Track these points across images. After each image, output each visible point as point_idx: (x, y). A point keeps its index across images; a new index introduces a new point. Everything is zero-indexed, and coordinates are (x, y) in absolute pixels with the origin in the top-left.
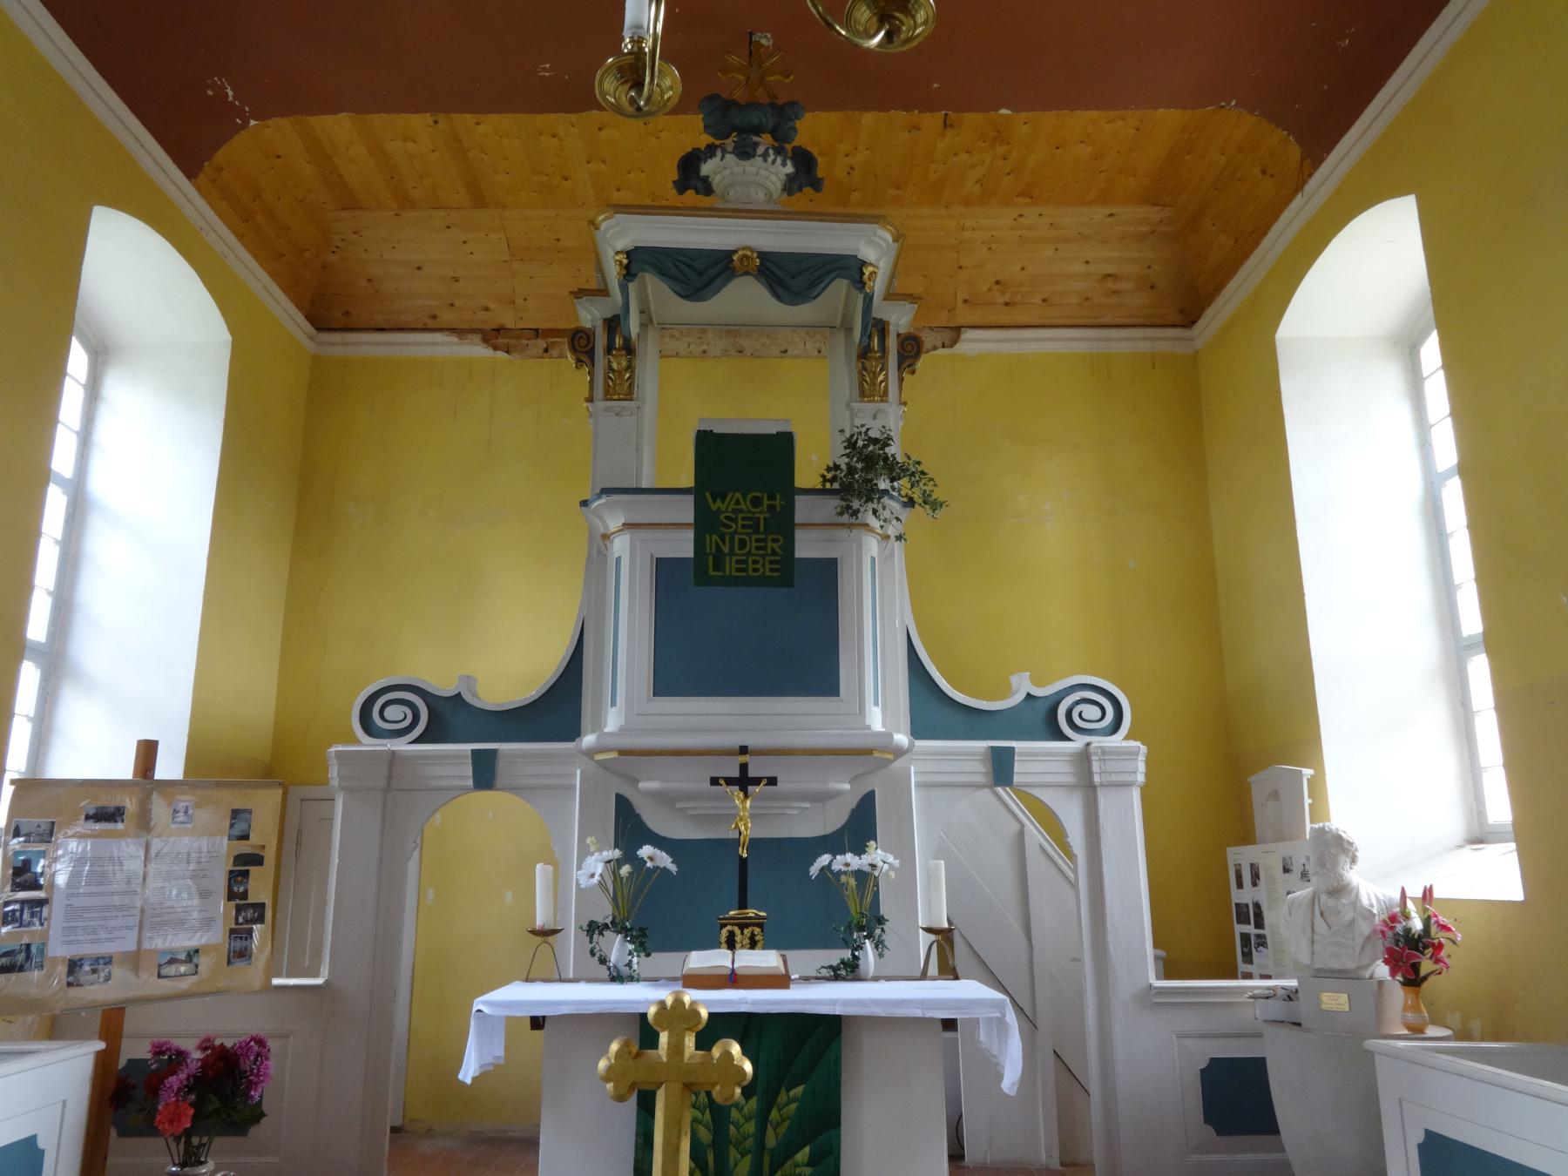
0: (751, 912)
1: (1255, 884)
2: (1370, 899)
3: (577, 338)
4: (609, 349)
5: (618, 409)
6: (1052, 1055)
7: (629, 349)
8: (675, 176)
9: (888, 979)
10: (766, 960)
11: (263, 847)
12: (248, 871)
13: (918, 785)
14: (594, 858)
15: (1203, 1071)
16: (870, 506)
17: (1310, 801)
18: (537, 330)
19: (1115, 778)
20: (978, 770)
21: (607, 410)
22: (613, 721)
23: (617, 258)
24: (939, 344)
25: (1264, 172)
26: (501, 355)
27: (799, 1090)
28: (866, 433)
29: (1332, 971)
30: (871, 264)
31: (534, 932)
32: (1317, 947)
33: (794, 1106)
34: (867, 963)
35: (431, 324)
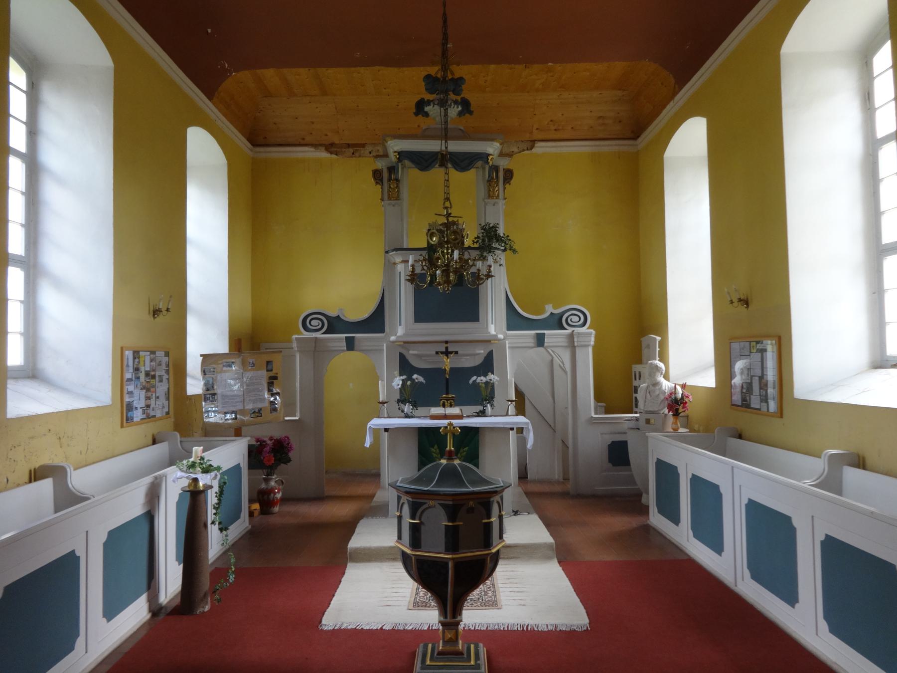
0: (450, 396)
1: (640, 379)
2: (665, 387)
3: (376, 173)
4: (390, 179)
5: (393, 204)
6: (561, 441)
7: (397, 180)
8: (414, 111)
9: (495, 416)
10: (456, 410)
11: (277, 374)
12: (273, 382)
13: (509, 347)
14: (397, 379)
15: (609, 445)
16: (490, 254)
17: (659, 349)
18: (349, 144)
19: (583, 343)
20: (531, 342)
21: (389, 204)
22: (400, 331)
23: (394, 154)
24: (526, 148)
25: (662, 84)
26: (334, 156)
27: (466, 448)
28: (489, 225)
29: (650, 411)
30: (491, 155)
31: (380, 403)
32: (646, 403)
33: (465, 453)
34: (488, 411)
35: (302, 142)
